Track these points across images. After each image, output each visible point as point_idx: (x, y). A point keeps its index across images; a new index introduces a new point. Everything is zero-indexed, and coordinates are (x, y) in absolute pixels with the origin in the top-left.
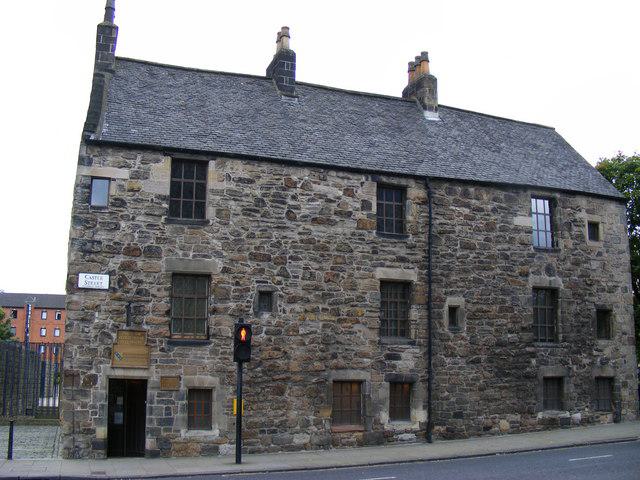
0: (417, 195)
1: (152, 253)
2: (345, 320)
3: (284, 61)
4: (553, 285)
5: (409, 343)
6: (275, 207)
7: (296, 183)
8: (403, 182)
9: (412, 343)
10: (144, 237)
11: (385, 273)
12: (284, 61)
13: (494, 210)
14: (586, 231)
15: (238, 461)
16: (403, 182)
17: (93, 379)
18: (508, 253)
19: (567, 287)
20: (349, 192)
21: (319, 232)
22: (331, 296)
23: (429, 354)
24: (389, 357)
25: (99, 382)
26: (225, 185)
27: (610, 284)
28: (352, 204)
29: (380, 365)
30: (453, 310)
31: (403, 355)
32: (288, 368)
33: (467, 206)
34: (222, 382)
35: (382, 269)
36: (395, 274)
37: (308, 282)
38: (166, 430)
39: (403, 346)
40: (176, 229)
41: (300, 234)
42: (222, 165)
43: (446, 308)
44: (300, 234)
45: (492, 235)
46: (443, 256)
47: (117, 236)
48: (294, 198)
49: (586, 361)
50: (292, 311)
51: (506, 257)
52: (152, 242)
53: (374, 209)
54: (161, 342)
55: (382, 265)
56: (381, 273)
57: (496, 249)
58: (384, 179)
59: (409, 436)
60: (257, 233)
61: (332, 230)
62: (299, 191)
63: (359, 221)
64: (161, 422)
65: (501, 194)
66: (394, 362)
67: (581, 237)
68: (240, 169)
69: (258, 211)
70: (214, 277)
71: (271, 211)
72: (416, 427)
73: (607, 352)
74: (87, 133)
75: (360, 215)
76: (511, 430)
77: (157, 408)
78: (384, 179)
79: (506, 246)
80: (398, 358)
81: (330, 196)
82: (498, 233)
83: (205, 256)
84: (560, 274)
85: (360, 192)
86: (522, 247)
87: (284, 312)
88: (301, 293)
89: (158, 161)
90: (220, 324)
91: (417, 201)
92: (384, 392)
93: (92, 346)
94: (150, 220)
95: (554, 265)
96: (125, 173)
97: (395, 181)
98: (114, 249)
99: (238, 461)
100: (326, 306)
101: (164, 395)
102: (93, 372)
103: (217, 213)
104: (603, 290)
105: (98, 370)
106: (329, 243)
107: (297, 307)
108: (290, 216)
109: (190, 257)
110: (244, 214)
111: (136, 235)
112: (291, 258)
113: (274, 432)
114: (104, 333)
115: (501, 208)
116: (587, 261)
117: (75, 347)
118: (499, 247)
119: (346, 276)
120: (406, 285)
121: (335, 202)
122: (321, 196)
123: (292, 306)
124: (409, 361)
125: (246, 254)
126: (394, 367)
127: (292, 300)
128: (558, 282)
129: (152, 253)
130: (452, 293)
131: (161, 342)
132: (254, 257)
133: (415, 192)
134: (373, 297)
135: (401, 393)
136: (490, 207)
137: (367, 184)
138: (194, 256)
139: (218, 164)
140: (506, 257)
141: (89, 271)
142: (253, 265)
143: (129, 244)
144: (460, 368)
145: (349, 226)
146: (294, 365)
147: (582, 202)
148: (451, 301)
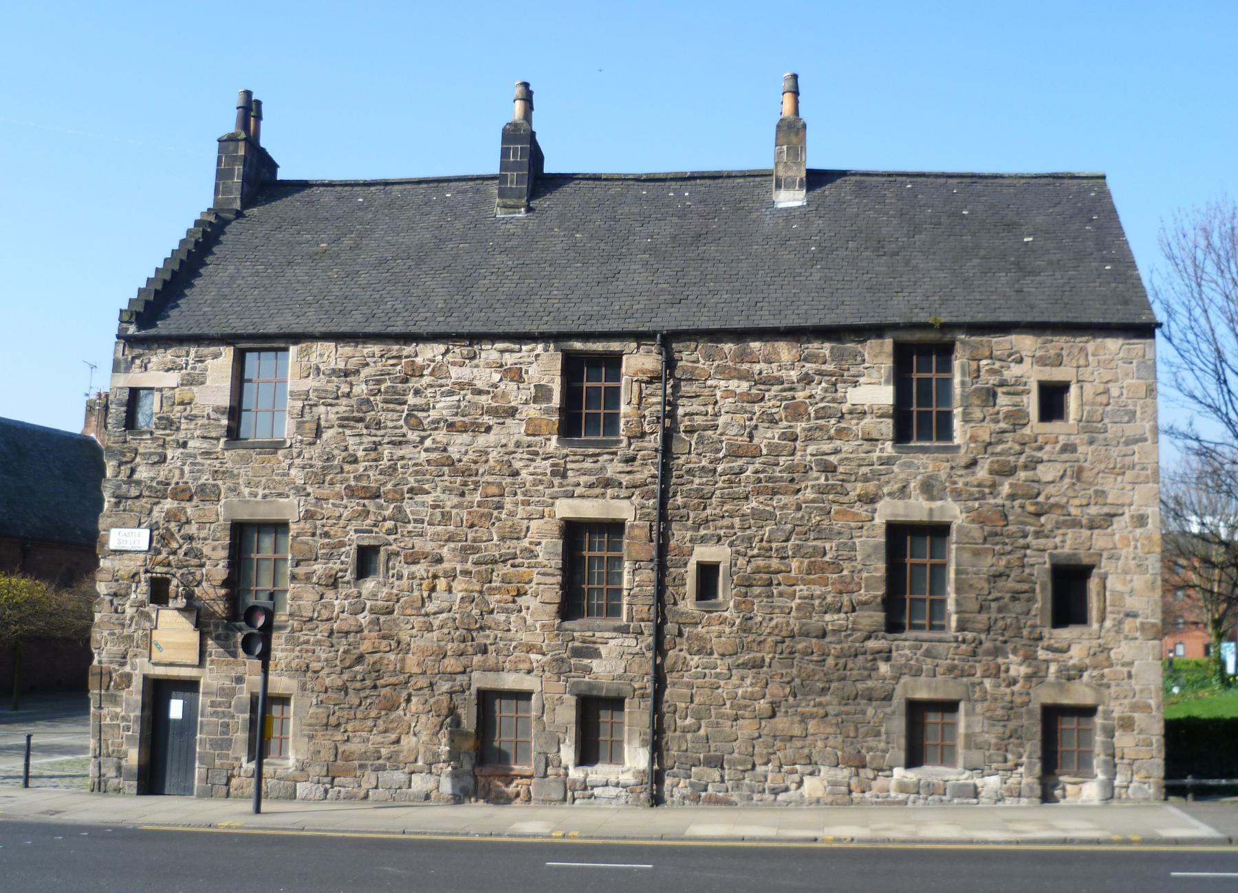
0: (640, 366)
1: (208, 494)
2: (498, 589)
3: (522, 143)
4: (936, 518)
5: (617, 629)
6: (388, 410)
7: (423, 368)
8: (615, 346)
9: (624, 630)
10: (197, 471)
11: (571, 507)
12: (522, 143)
13: (807, 380)
14: (1032, 403)
15: (258, 810)
16: (615, 346)
17: (128, 678)
18: (832, 458)
19: (973, 521)
20: (516, 375)
21: (458, 444)
22: (478, 550)
23: (659, 647)
24: (577, 653)
25: (134, 683)
26: (311, 383)
27: (1093, 510)
28: (515, 394)
29: (560, 666)
30: (707, 573)
31: (603, 650)
32: (403, 668)
33: (742, 377)
34: (303, 687)
35: (570, 501)
36: (590, 509)
37: (440, 528)
38: (220, 757)
39: (607, 635)
40: (242, 457)
41: (426, 450)
42: (304, 354)
43: (692, 567)
44: (426, 450)
45: (800, 427)
46: (689, 471)
47: (163, 472)
48: (417, 392)
49: (1018, 669)
50: (412, 577)
51: (829, 469)
52: (205, 478)
53: (556, 400)
54: (217, 626)
55: (571, 496)
56: (566, 509)
57: (807, 453)
58: (578, 345)
59: (612, 791)
60: (360, 454)
61: (482, 440)
62: (427, 380)
63: (530, 421)
64: (215, 744)
66: (586, 661)
67: (1017, 418)
68: (328, 355)
69: (361, 420)
70: (292, 526)
71: (383, 416)
72: (628, 778)
73: (1076, 655)
74: (125, 325)
75: (532, 411)
76: (830, 799)
77: (209, 724)
78: (578, 345)
79: (827, 447)
80: (596, 654)
81: (479, 384)
82: (813, 423)
83: (280, 495)
84: (957, 495)
85: (534, 373)
86: (867, 446)
87: (400, 577)
88: (429, 547)
89: (216, 356)
90: (300, 598)
91: (641, 377)
92: (567, 714)
93: (126, 632)
94: (205, 445)
95: (943, 475)
96: (173, 379)
97: (599, 346)
98: (160, 491)
99: (258, 810)
100: (469, 566)
101: (220, 705)
102: (127, 669)
103: (298, 428)
104: (1075, 524)
105: (134, 667)
106: (475, 462)
107: (420, 569)
108: (413, 421)
109: (259, 498)
110: (340, 426)
111: (187, 469)
112: (411, 490)
113: (382, 768)
114: (142, 612)
115: (821, 373)
116: (1032, 464)
117: (106, 633)
118: (811, 449)
119: (503, 516)
120: (615, 528)
121: (488, 392)
122: (462, 386)
123: (414, 568)
124: (615, 658)
125: (339, 488)
126: (588, 670)
127: (413, 560)
128: (953, 512)
129: (208, 494)
130: (704, 540)
131: (217, 626)
132: (352, 492)
133: (639, 361)
134: (549, 552)
135: (594, 718)
136: (794, 375)
137: (544, 356)
138: (265, 496)
139: (300, 352)
140: (829, 469)
141: (124, 525)
142: (354, 505)
143: (177, 483)
144: (718, 676)
145: (516, 429)
146: (412, 663)
147: (1026, 343)
148: (705, 553)
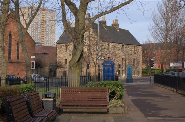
65: (131, 46)
